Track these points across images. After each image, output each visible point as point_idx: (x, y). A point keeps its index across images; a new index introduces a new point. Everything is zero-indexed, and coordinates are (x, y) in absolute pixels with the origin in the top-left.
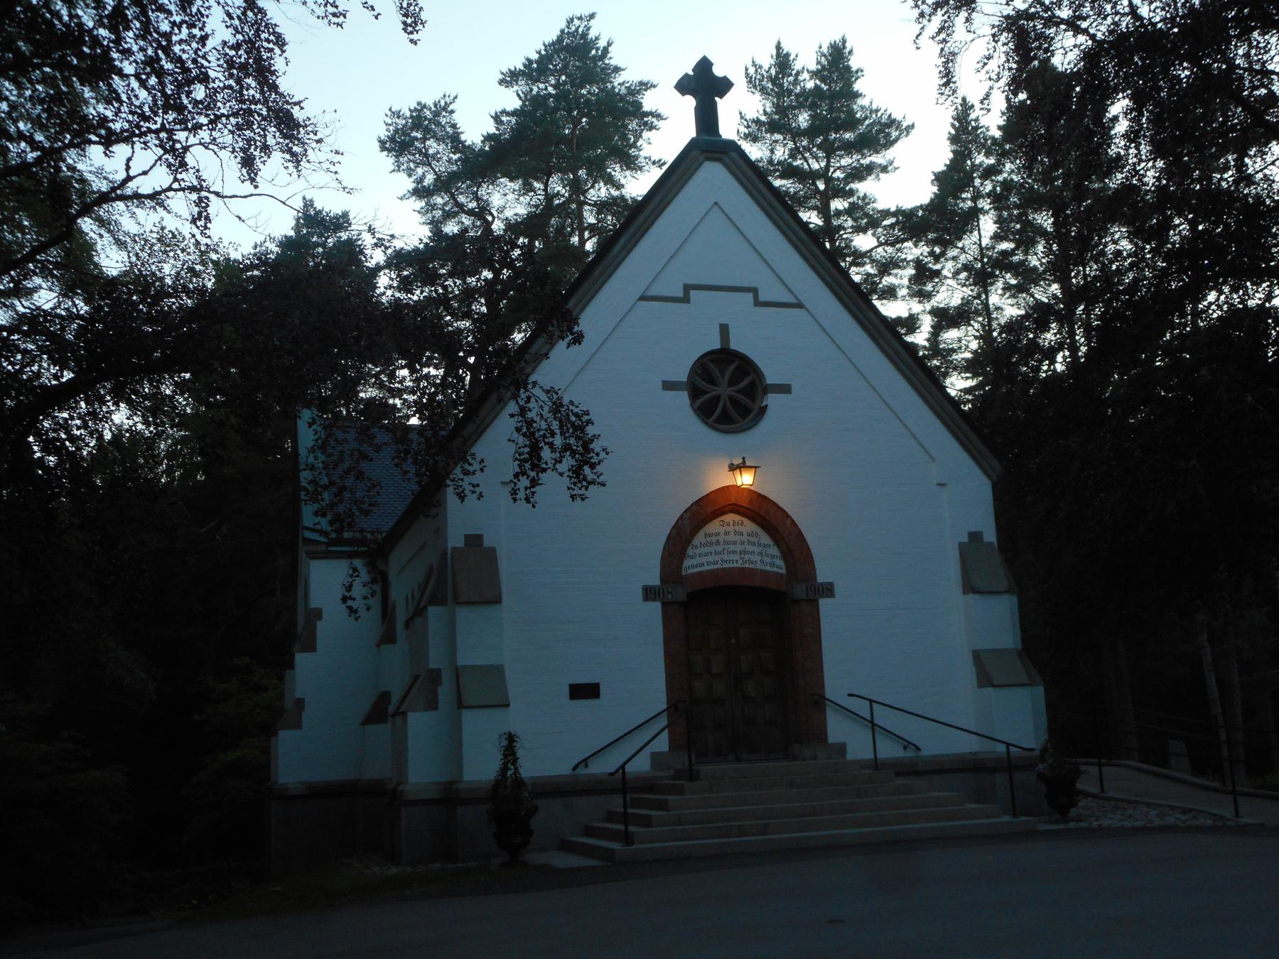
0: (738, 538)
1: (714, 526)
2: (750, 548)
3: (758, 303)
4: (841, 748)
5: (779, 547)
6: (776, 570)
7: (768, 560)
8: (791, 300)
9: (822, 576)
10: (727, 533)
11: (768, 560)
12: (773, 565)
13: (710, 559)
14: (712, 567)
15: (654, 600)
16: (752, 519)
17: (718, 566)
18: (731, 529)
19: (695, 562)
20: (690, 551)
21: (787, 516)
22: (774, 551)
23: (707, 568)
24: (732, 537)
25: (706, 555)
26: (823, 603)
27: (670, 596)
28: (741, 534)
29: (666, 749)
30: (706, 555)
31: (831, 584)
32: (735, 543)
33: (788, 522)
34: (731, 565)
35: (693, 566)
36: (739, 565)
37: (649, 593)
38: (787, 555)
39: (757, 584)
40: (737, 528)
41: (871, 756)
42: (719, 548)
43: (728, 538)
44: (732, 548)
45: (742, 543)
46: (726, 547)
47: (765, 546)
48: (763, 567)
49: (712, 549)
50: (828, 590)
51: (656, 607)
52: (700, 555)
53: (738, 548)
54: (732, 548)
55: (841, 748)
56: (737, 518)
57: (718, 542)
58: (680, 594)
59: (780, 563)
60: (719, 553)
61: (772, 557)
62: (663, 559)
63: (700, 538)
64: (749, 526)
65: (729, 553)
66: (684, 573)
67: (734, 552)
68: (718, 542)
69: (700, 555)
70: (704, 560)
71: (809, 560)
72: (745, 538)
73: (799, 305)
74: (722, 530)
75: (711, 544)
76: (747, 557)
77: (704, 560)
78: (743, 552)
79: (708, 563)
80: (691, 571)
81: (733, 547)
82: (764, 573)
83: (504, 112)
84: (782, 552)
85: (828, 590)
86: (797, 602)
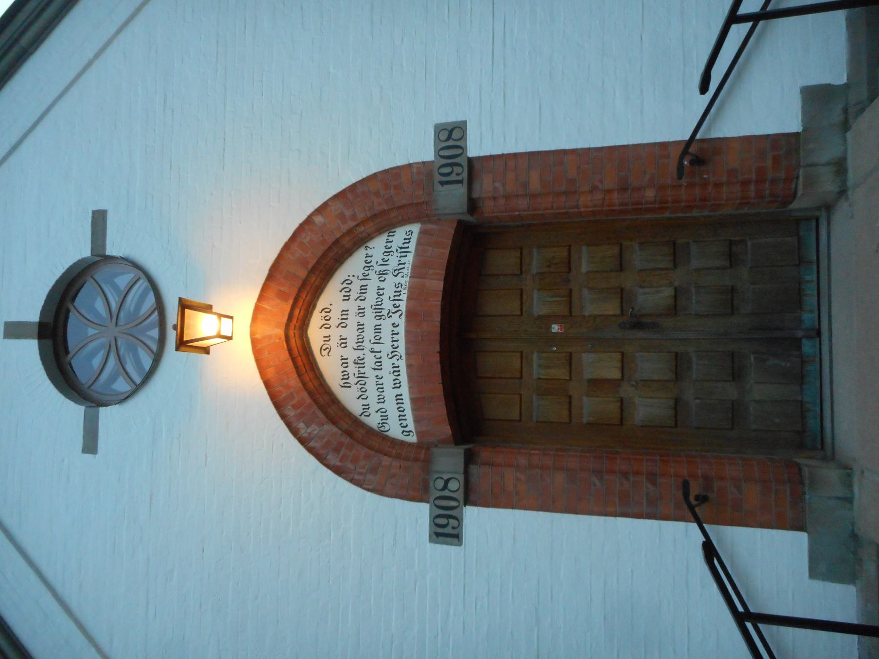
1: (330, 367)
2: (371, 297)
4: (816, 97)
5: (369, 237)
6: (412, 246)
7: (393, 261)
9: (422, 150)
10: (343, 343)
11: (393, 261)
14: (404, 378)
15: (459, 520)
16: (318, 291)
17: (402, 364)
18: (335, 333)
19: (391, 406)
20: (373, 421)
21: (308, 221)
22: (378, 245)
23: (405, 390)
24: (351, 333)
25: (380, 388)
26: (476, 148)
28: (344, 313)
29: (802, 538)
30: (380, 388)
31: (440, 129)
32: (361, 327)
33: (319, 219)
34: (402, 337)
35: (402, 418)
36: (402, 322)
38: (384, 223)
39: (439, 285)
40: (334, 322)
41: (96, 277)
42: (370, 360)
43: (352, 342)
44: (369, 334)
45: (361, 312)
46: (367, 345)
47: (368, 266)
48: (407, 271)
49: (371, 374)
50: (451, 136)
52: (381, 400)
53: (370, 320)
54: (369, 334)
55: (816, 97)
56: (316, 319)
58: (449, 462)
59: (400, 234)
60: (379, 363)
61: (388, 252)
63: (350, 399)
64: (331, 296)
66: (413, 439)
67: (377, 329)
69: (381, 400)
70: (390, 394)
71: (390, 177)
72: (352, 306)
74: (337, 352)
75: (362, 376)
76: (387, 305)
77: (390, 394)
78: (378, 308)
79: (397, 386)
80: (411, 427)
81: (370, 335)
84: (379, 231)
85: (451, 136)
86: (473, 205)
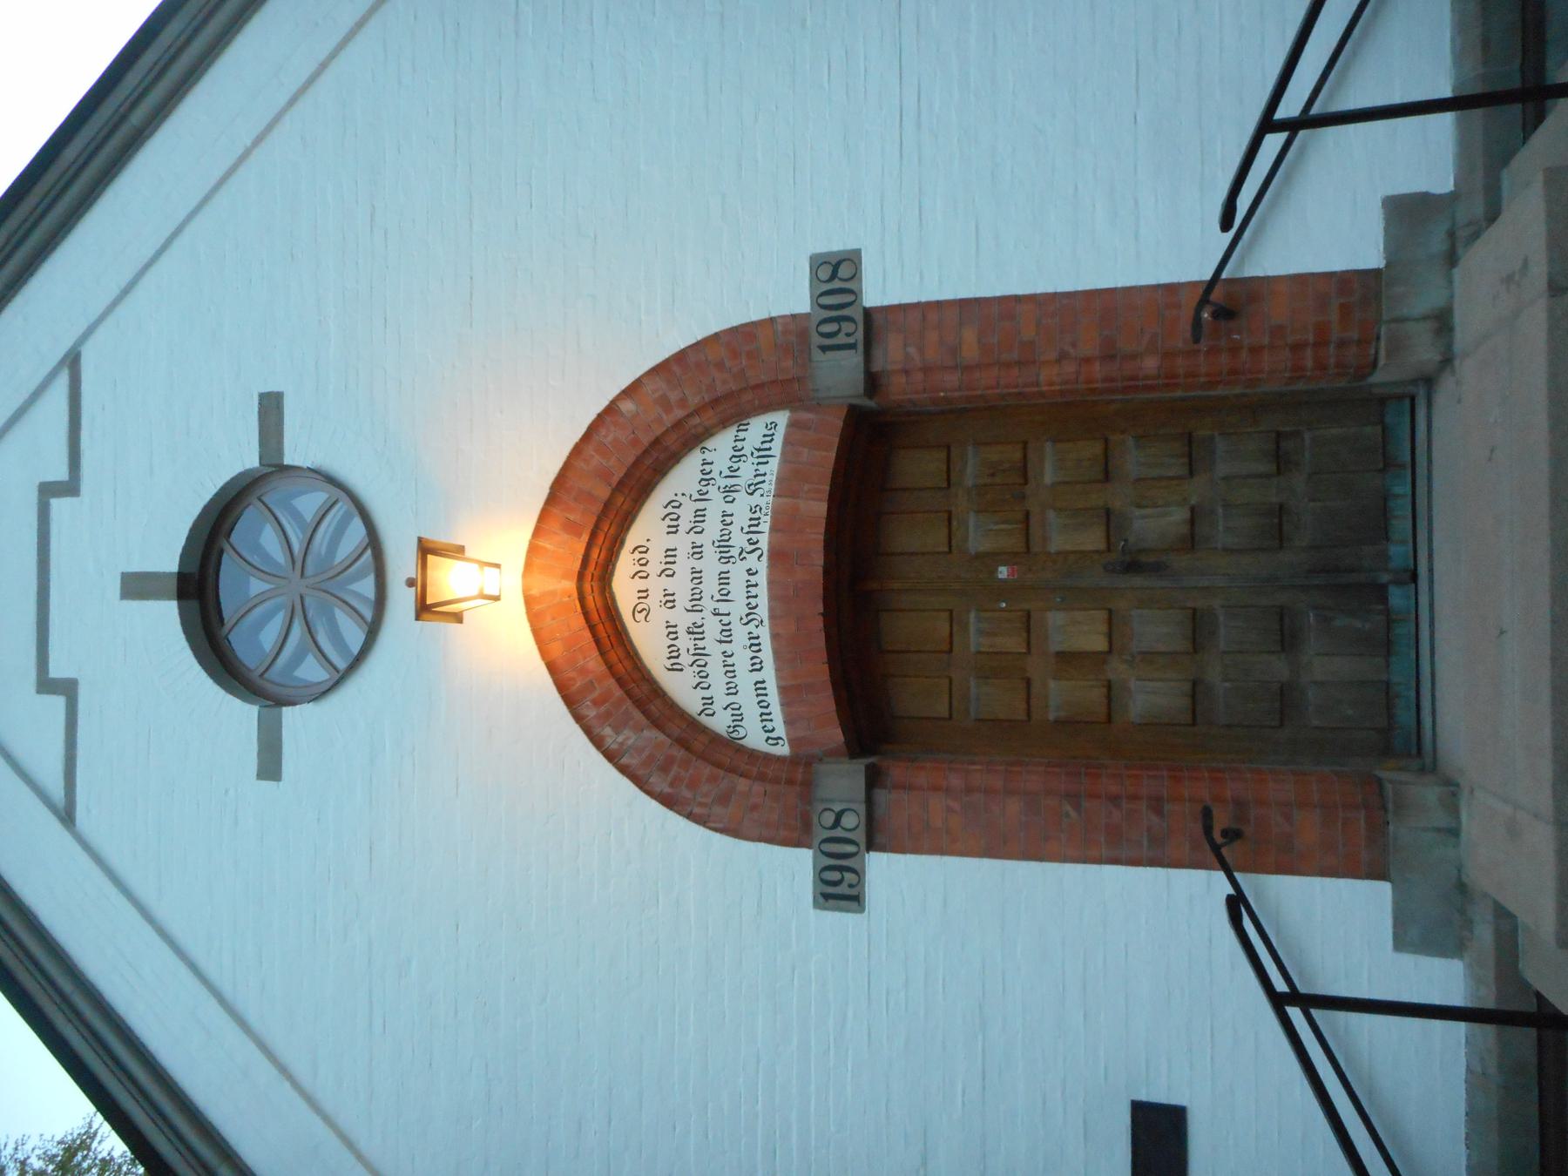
0: (683, 565)
2: (713, 527)
3: (48, 491)
4: (1406, 213)
5: (708, 433)
6: (777, 447)
7: (747, 471)
8: (63, 381)
10: (669, 601)
11: (747, 471)
12: (763, 454)
13: (742, 659)
14: (767, 655)
15: (859, 873)
18: (656, 586)
19: (751, 711)
20: (720, 723)
21: (611, 410)
22: (721, 445)
23: (769, 674)
24: (681, 586)
25: (730, 671)
26: (876, 292)
27: (849, 821)
28: (670, 553)
29: (1385, 888)
30: (730, 671)
31: (818, 262)
32: (697, 575)
33: (627, 407)
34: (763, 591)
35: (765, 716)
36: (762, 567)
37: (839, 890)
38: (731, 410)
39: (821, 508)
40: (654, 568)
42: (712, 627)
43: (683, 600)
44: (710, 586)
45: (697, 551)
46: (708, 604)
47: (706, 478)
48: (770, 486)
50: (836, 273)
51: (884, 872)
52: (732, 690)
53: (711, 565)
55: (1406, 213)
56: (625, 564)
57: (696, 631)
58: (842, 783)
59: (757, 427)
60: (726, 630)
61: (738, 456)
62: (733, 830)
63: (681, 688)
64: (648, 528)
65: (725, 598)
66: (783, 750)
67: (724, 578)
68: (696, 631)
69: (732, 690)
70: (745, 680)
71: (739, 342)
72: (683, 542)
73: (72, 361)
74: (660, 615)
75: (700, 653)
76: (739, 540)
77: (745, 680)
79: (757, 667)
80: (781, 731)
82: (786, 487)
83: (320, 693)
84: (724, 424)
85: (836, 273)
86: (873, 382)
